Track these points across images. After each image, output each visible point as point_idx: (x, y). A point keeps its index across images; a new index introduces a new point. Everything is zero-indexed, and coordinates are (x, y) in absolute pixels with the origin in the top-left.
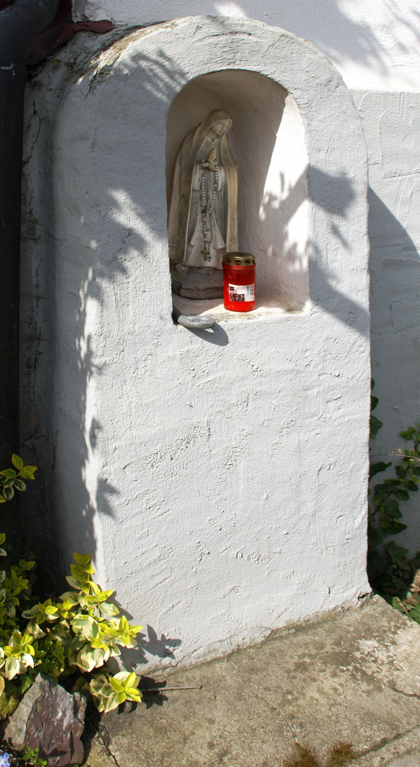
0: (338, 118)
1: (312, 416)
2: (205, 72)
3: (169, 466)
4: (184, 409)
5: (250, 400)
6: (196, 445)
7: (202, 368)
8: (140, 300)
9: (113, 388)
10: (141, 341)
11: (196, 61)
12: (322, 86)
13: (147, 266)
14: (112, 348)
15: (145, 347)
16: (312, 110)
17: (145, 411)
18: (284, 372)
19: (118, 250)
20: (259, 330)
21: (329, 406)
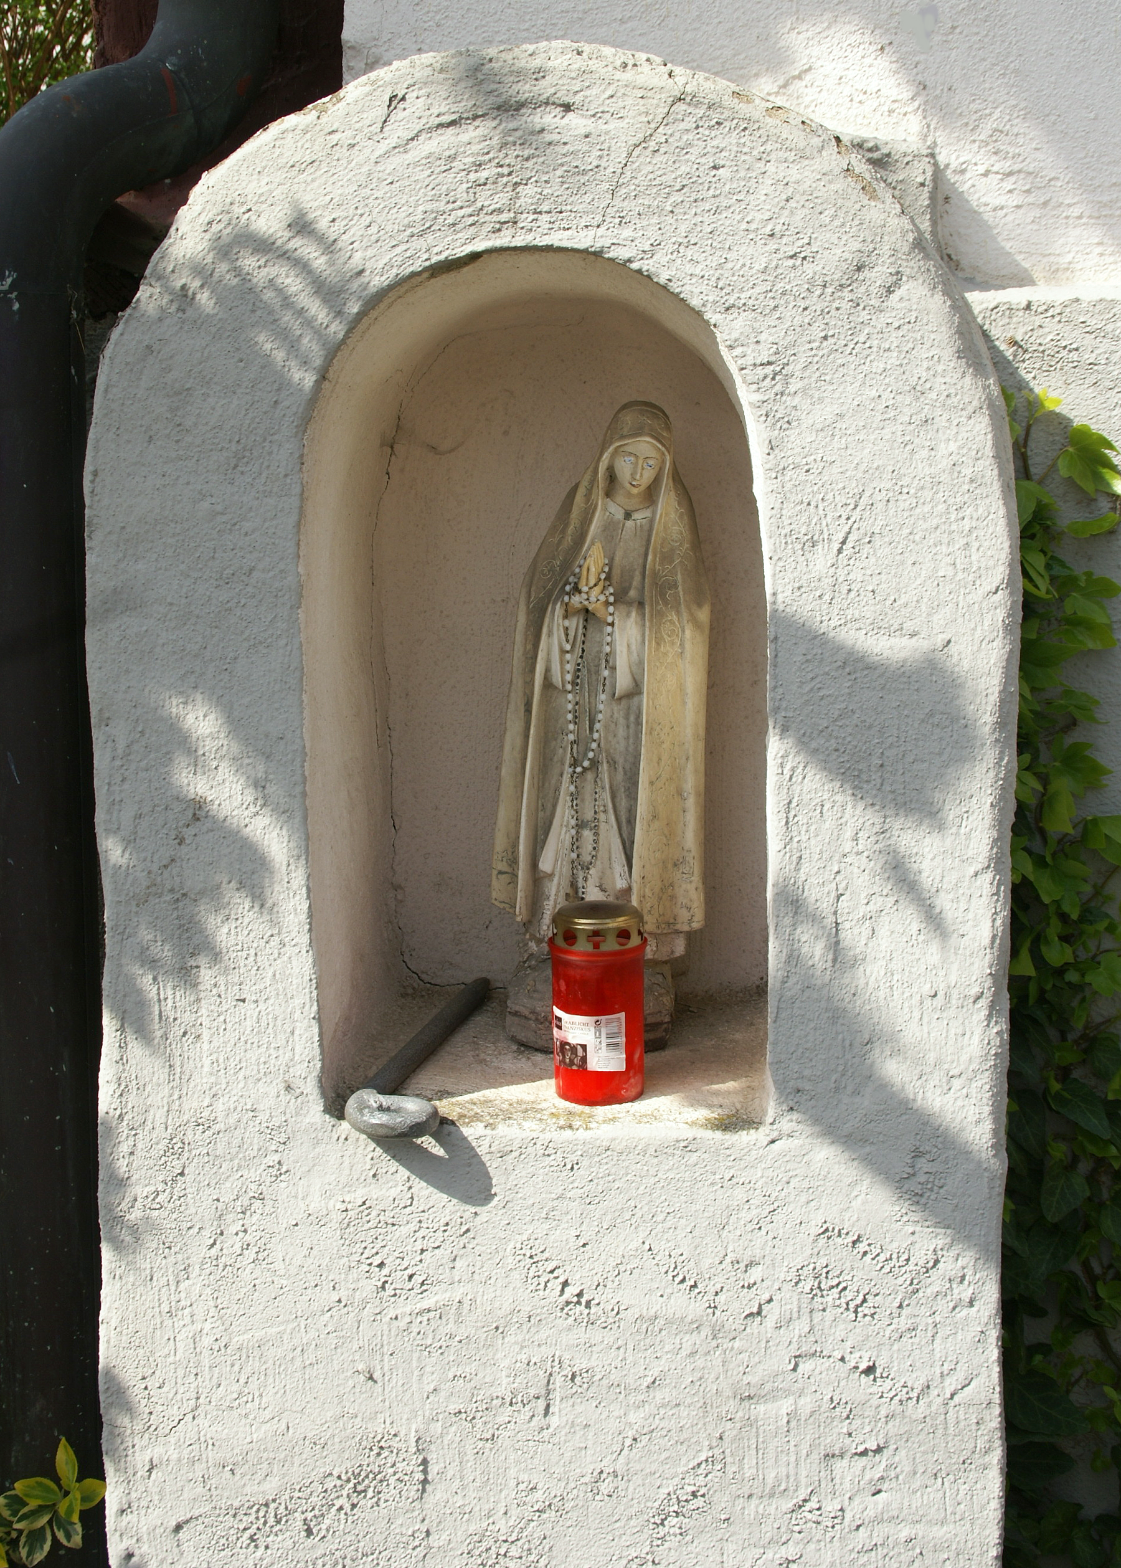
0: (891, 413)
1: (772, 1495)
2: (417, 266)
3: (301, 1554)
4: (351, 1383)
5: (556, 1395)
6: (382, 1505)
7: (405, 1264)
8: (229, 1026)
9: (155, 1283)
10: (234, 1151)
11: (389, 228)
12: (829, 290)
13: (246, 920)
14: (152, 1162)
15: (245, 1172)
16: (792, 389)
17: (236, 1368)
18: (668, 1322)
19: (164, 862)
20: (577, 1157)
21: (837, 1473)
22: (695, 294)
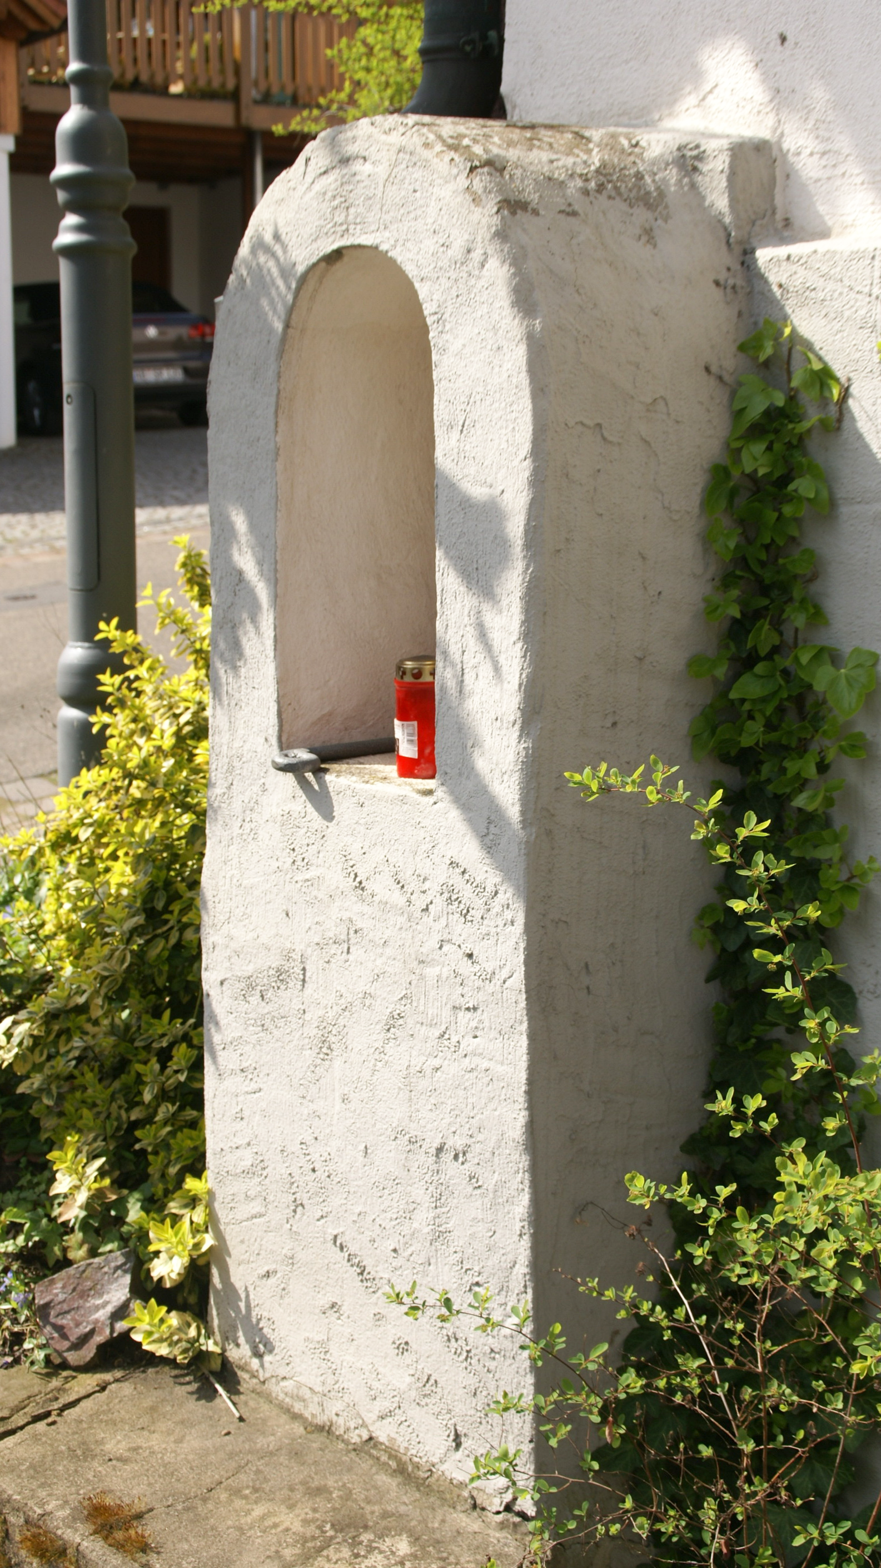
22: (410, 270)
